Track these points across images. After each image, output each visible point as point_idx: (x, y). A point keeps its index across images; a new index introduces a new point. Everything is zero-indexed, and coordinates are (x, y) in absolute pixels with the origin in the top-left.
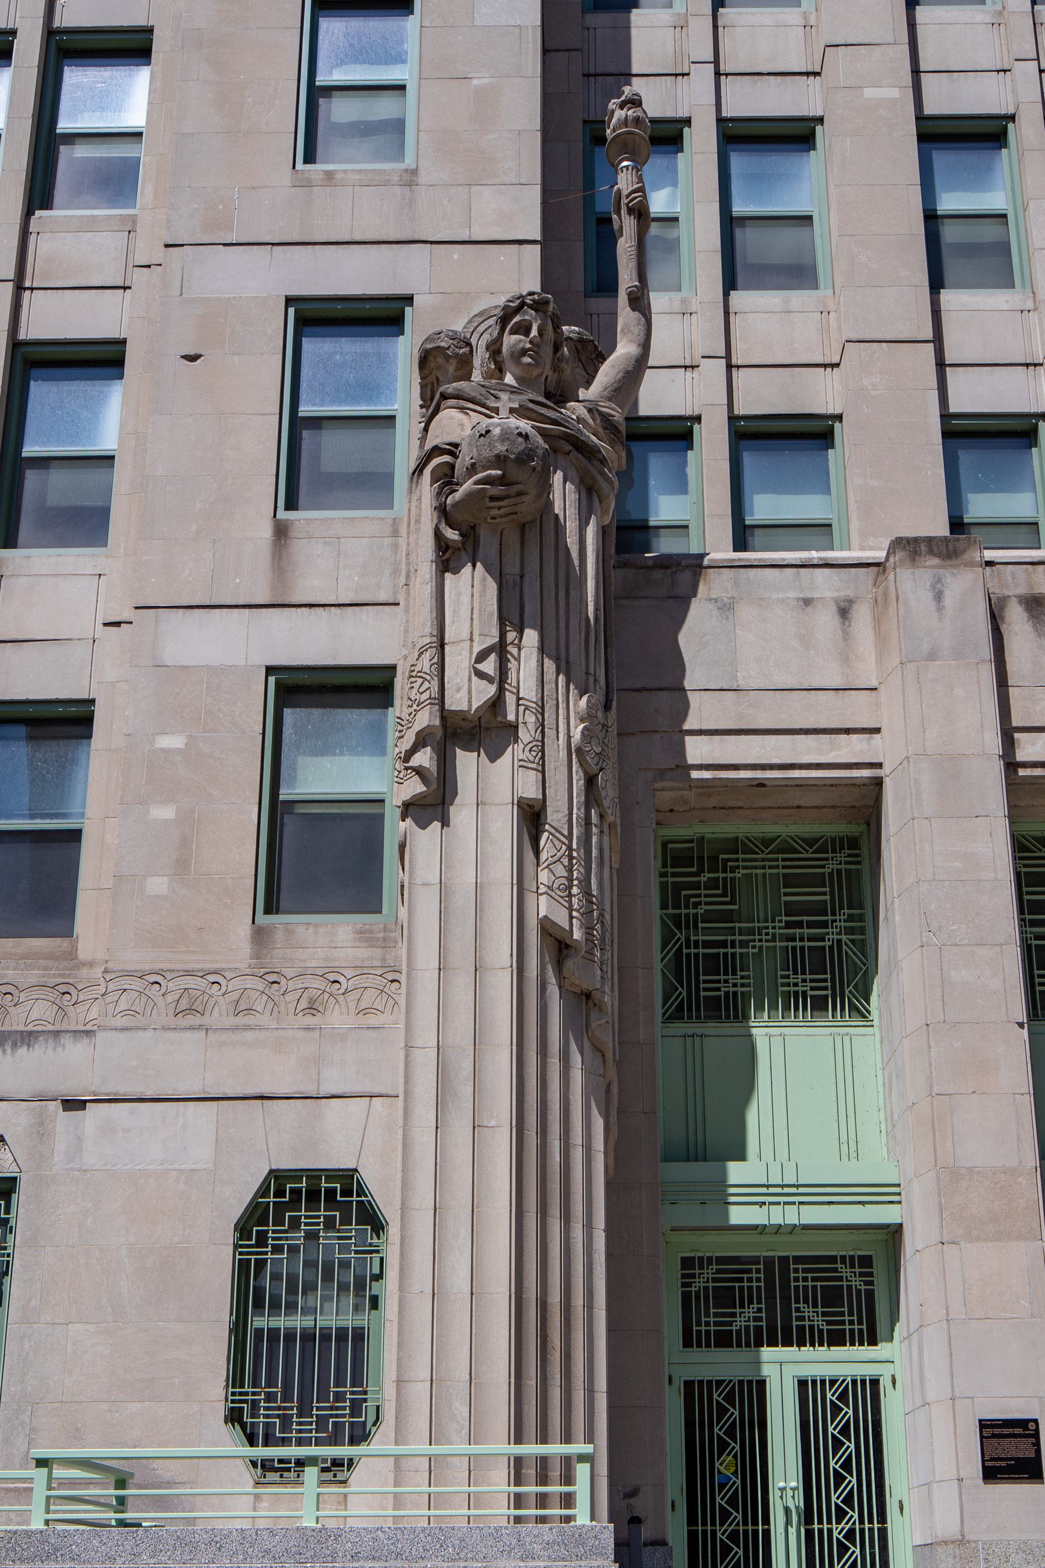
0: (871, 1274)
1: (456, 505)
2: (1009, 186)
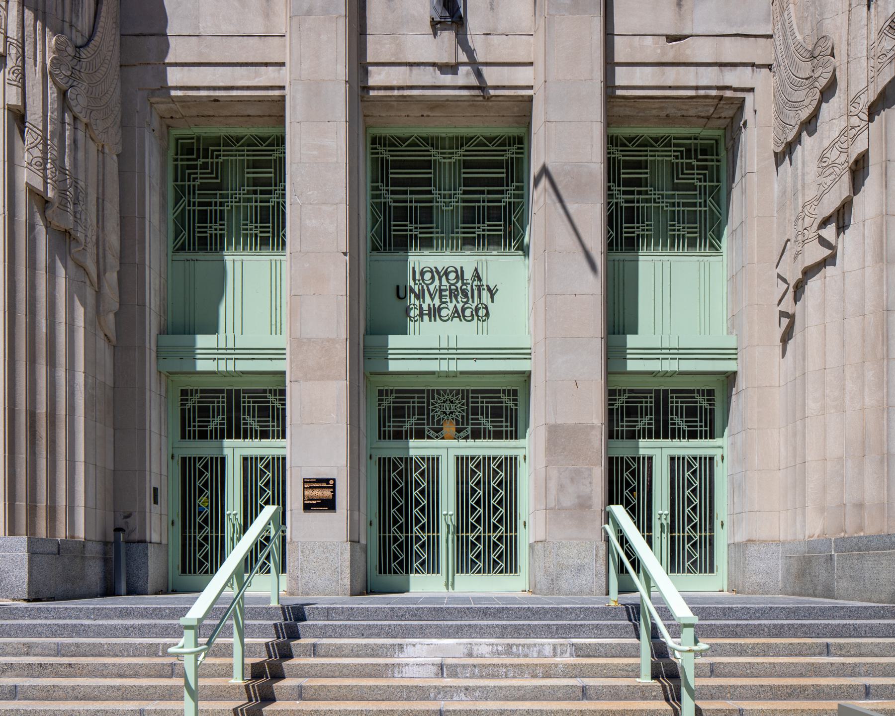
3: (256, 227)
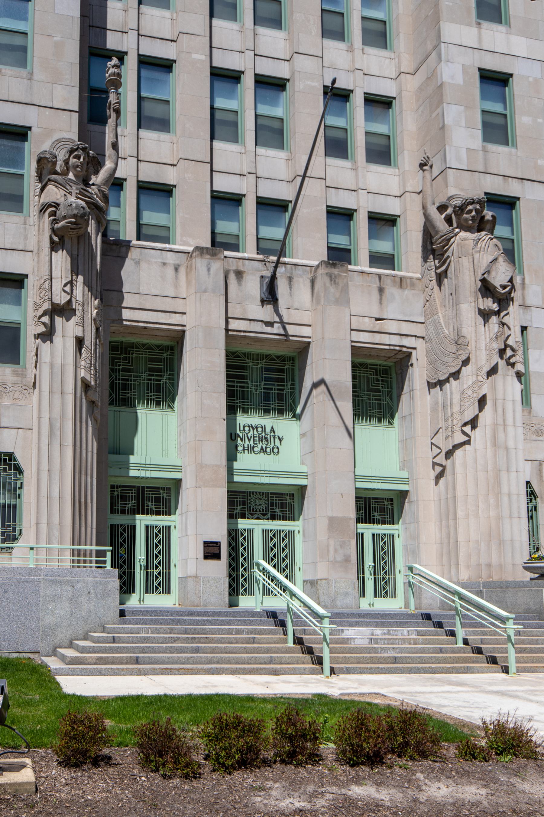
0: (170, 493)
1: (58, 229)
2: (239, 100)
3: (154, 395)
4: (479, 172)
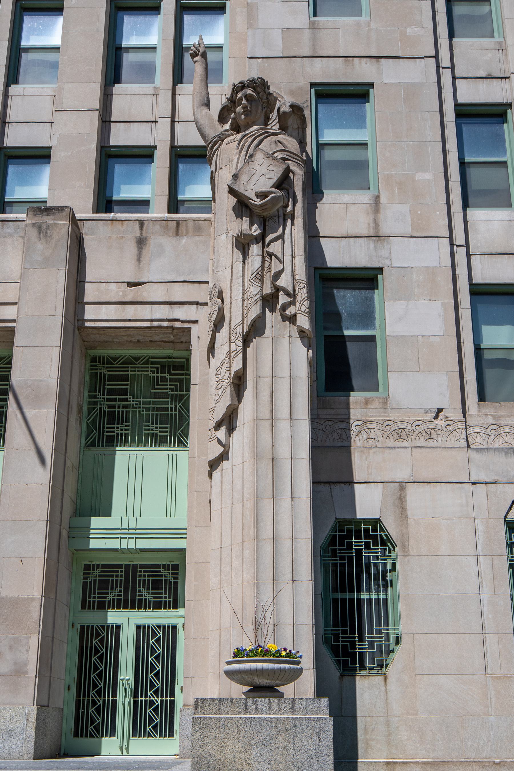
0: (177, 574)
4: (302, 57)
